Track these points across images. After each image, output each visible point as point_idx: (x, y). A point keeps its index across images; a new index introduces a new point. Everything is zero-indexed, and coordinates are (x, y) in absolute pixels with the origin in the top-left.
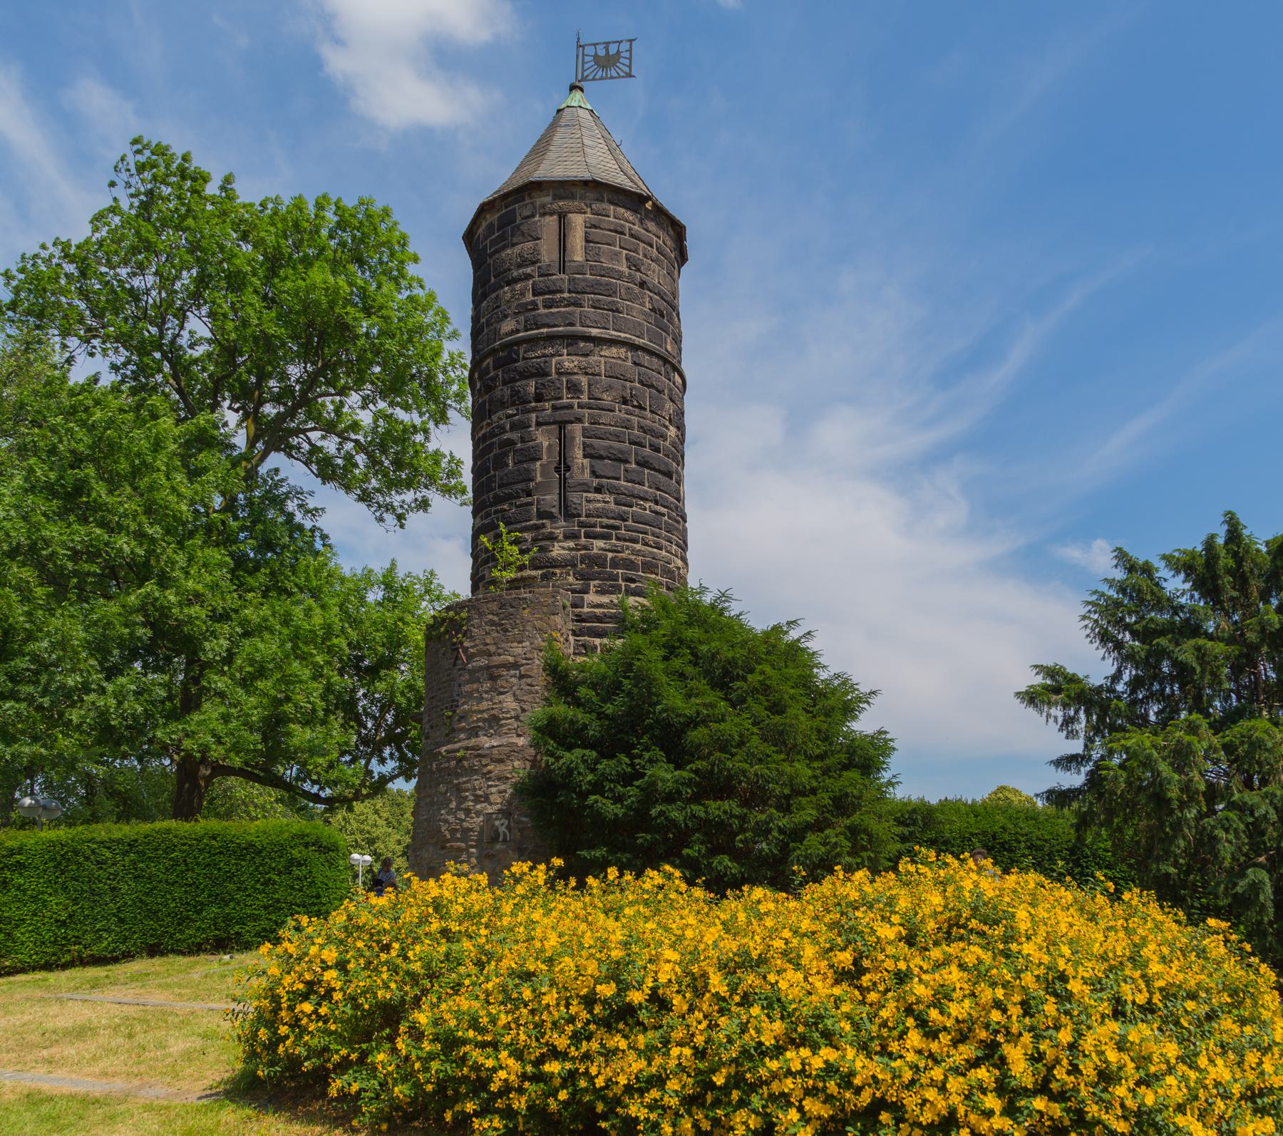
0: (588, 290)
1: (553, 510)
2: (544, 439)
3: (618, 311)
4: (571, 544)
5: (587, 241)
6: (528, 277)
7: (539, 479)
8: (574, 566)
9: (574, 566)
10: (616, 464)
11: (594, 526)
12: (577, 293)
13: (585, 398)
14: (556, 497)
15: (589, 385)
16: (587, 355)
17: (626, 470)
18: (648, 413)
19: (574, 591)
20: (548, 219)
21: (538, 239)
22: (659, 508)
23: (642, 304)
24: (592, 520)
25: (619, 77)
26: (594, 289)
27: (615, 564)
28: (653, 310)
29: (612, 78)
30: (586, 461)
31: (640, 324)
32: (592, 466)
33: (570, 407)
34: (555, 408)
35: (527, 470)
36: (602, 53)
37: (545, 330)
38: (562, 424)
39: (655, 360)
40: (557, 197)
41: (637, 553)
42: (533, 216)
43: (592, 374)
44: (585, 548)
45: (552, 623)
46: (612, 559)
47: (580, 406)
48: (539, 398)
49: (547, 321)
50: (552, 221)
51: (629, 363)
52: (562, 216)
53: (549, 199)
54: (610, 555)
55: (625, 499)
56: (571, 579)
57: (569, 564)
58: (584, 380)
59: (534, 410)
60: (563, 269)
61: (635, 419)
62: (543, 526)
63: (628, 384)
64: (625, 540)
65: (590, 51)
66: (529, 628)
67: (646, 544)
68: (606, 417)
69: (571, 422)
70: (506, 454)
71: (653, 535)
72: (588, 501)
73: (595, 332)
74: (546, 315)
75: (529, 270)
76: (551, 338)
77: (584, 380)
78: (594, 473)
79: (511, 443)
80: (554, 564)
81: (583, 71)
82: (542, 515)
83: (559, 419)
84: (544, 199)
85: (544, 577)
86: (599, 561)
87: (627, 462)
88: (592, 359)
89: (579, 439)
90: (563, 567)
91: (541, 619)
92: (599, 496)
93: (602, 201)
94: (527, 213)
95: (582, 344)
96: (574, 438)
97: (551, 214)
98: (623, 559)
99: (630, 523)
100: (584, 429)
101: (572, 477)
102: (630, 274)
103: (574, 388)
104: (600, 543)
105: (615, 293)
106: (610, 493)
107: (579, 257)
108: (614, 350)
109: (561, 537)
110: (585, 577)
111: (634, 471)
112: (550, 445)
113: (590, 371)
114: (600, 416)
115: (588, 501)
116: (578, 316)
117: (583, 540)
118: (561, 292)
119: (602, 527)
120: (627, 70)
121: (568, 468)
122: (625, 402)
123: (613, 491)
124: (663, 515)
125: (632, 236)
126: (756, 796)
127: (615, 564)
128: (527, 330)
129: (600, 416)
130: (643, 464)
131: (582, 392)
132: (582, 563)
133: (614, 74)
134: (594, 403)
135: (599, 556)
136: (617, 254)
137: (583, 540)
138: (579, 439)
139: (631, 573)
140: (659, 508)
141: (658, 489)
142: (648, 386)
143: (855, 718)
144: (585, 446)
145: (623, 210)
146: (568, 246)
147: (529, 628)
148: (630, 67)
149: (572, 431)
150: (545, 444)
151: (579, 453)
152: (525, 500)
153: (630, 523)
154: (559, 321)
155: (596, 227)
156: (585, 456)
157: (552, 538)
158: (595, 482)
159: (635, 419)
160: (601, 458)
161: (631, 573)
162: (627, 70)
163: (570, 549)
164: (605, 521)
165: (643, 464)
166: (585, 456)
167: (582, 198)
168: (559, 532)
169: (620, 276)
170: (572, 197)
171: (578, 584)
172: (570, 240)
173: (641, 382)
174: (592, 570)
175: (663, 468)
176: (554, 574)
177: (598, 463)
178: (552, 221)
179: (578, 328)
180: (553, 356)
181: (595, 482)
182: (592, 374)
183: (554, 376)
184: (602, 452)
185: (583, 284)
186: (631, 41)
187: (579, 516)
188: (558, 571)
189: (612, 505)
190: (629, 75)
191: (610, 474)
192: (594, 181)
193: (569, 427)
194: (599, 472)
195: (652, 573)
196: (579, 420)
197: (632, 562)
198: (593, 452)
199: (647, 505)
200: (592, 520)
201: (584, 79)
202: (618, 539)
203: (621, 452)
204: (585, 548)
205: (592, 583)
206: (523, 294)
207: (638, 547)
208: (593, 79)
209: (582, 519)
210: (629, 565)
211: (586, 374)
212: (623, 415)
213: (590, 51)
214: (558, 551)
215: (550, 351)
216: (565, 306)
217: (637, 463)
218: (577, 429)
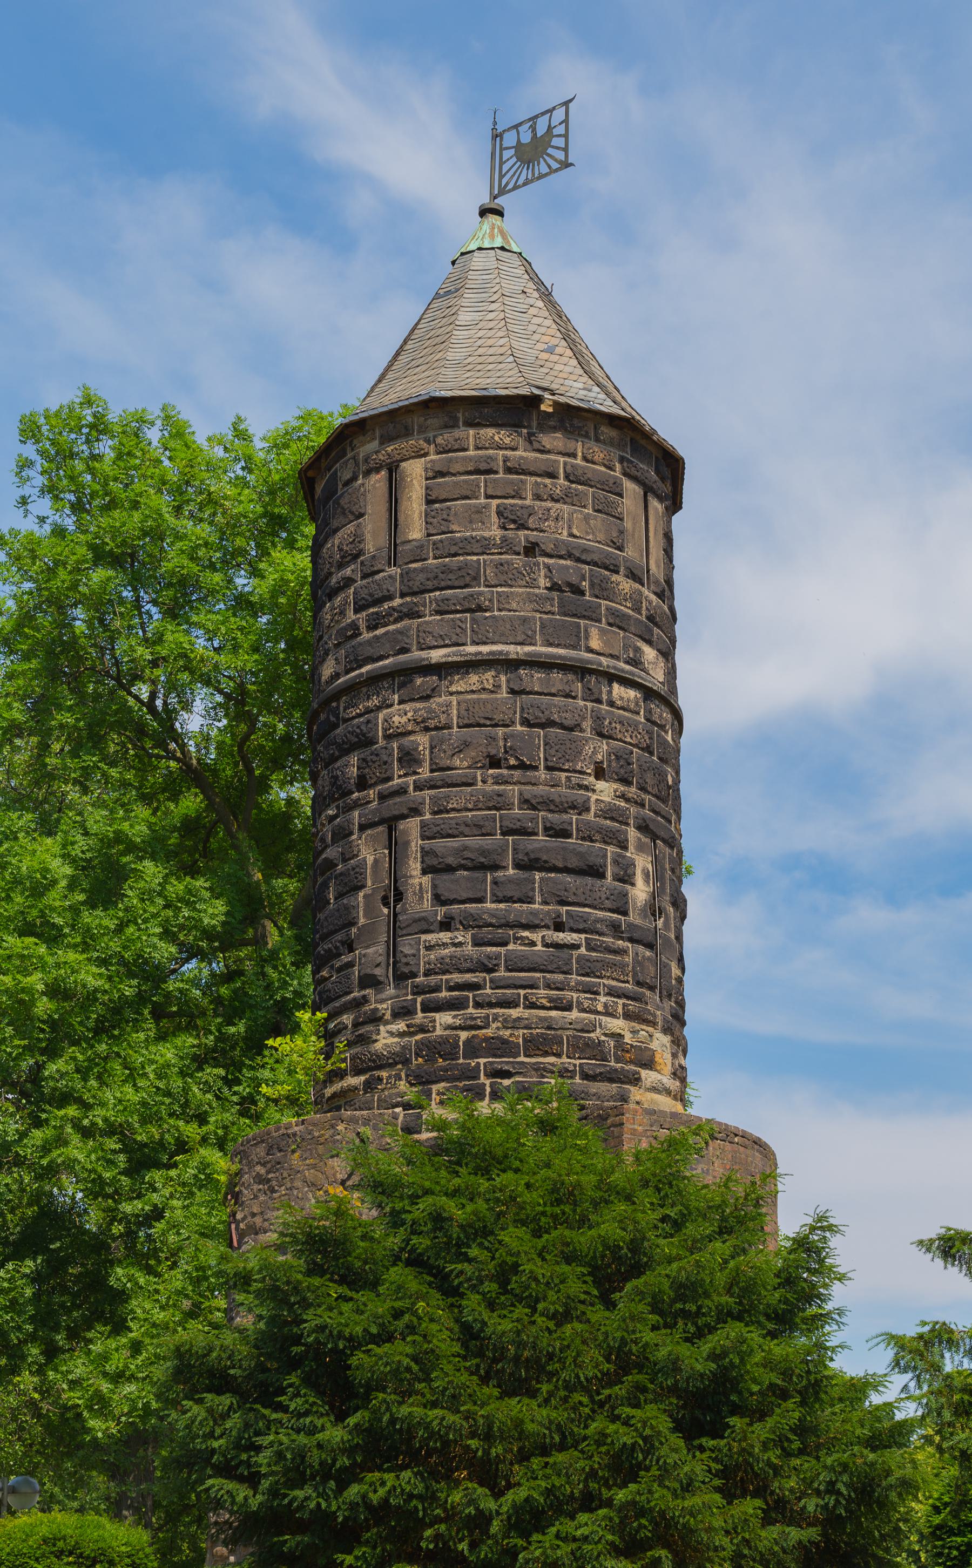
0: (430, 585)
1: (378, 971)
2: (369, 852)
3: (480, 609)
4: (401, 1026)
5: (429, 502)
6: (349, 581)
7: (362, 921)
8: (406, 1062)
9: (406, 1062)
10: (478, 874)
11: (437, 989)
12: (414, 594)
13: (425, 772)
14: (381, 949)
15: (432, 748)
16: (427, 698)
17: (495, 883)
18: (542, 774)
19: (407, 1106)
20: (375, 478)
21: (361, 515)
22: (561, 937)
23: (532, 584)
24: (433, 980)
25: (552, 171)
26: (439, 581)
27: (472, 1049)
28: (554, 587)
29: (541, 176)
30: (426, 880)
31: (525, 620)
32: (434, 886)
33: (402, 791)
34: (382, 797)
35: (347, 908)
36: (526, 138)
37: (368, 668)
38: (391, 823)
39: (556, 676)
40: (387, 439)
41: (515, 1024)
42: (354, 478)
43: (437, 728)
44: (422, 1029)
45: (329, 1172)
46: (468, 1042)
47: (418, 788)
48: (362, 784)
49: (369, 651)
50: (378, 480)
51: (504, 694)
52: (393, 469)
53: (375, 445)
54: (464, 1035)
55: (490, 932)
56: (403, 1085)
57: (399, 1059)
58: (422, 741)
59: (356, 805)
60: (393, 560)
61: (513, 791)
62: (365, 1000)
63: (500, 731)
64: (491, 1005)
65: (510, 139)
66: (298, 1184)
67: (533, 1006)
68: (458, 797)
69: (404, 817)
70: (325, 885)
71: (548, 986)
72: (429, 948)
73: (436, 655)
74: (369, 642)
75: (348, 572)
76: (374, 680)
77: (422, 741)
78: (439, 900)
79: (331, 864)
80: (379, 1063)
81: (501, 176)
82: (369, 981)
83: (386, 814)
84: (368, 448)
85: (369, 1086)
86: (443, 1049)
87: (496, 867)
88: (435, 703)
89: (416, 843)
90: (391, 1066)
91: (314, 1166)
92: (445, 936)
93: (455, 426)
94: (347, 476)
95: (419, 681)
96: (407, 843)
97: (377, 470)
98: (487, 1039)
99: (502, 973)
100: (424, 825)
101: (404, 910)
102: (504, 539)
103: (409, 759)
104: (445, 1018)
105: (476, 578)
106: (466, 928)
107: (415, 532)
108: (474, 678)
109: (388, 1016)
110: (423, 1080)
111: (510, 880)
112: (376, 861)
113: (431, 723)
114: (447, 798)
115: (429, 948)
116: (414, 632)
117: (420, 1017)
118: (390, 598)
119: (450, 989)
120: (560, 155)
121: (399, 896)
122: (495, 762)
123: (469, 923)
124: (576, 947)
125: (509, 470)
126: (438, 1458)
127: (472, 1049)
128: (347, 672)
129: (447, 798)
130: (528, 864)
131: (419, 763)
132: (417, 1055)
133: (544, 169)
134: (444, 779)
135: (444, 1040)
136: (479, 511)
137: (420, 1017)
138: (416, 843)
139: (502, 1062)
140: (561, 937)
141: (563, 903)
142: (542, 726)
143: (796, 1291)
144: (425, 853)
145: (490, 431)
146: (401, 518)
147: (298, 1184)
148: (566, 150)
149: (406, 832)
150: (370, 860)
151: (415, 867)
152: (345, 959)
153: (502, 973)
154: (386, 648)
155: (442, 474)
156: (424, 872)
157: (376, 1019)
158: (441, 911)
159: (513, 791)
160: (450, 869)
161: (502, 1062)
162: (560, 155)
163: (401, 1035)
164: (457, 978)
165: (528, 864)
166: (424, 872)
167: (422, 430)
168: (385, 1008)
169: (485, 546)
170: (407, 433)
171: (410, 1093)
172: (403, 505)
173: (526, 722)
174: (435, 1063)
175: (573, 863)
176: (380, 1079)
177: (445, 879)
178: (378, 480)
179: (416, 654)
180: (379, 708)
181: (441, 911)
182: (437, 728)
183: (381, 742)
184: (450, 860)
185: (421, 577)
186: (566, 104)
187: (414, 975)
188: (384, 1074)
189: (469, 949)
190: (566, 165)
191: (465, 895)
192: (433, 400)
193: (402, 825)
194: (446, 895)
195: (546, 1054)
196: (415, 811)
197: (505, 1042)
198: (434, 862)
199: (536, 936)
200: (433, 980)
201: (503, 191)
202: (478, 1005)
203: (483, 852)
204: (422, 1029)
205: (435, 1088)
206: (342, 613)
207: (515, 1013)
208: (516, 187)
209: (420, 979)
210: (500, 1047)
211: (427, 729)
212: (490, 788)
213: (510, 139)
214: (386, 1039)
215: (375, 701)
216: (396, 621)
217: (517, 866)
218: (412, 826)
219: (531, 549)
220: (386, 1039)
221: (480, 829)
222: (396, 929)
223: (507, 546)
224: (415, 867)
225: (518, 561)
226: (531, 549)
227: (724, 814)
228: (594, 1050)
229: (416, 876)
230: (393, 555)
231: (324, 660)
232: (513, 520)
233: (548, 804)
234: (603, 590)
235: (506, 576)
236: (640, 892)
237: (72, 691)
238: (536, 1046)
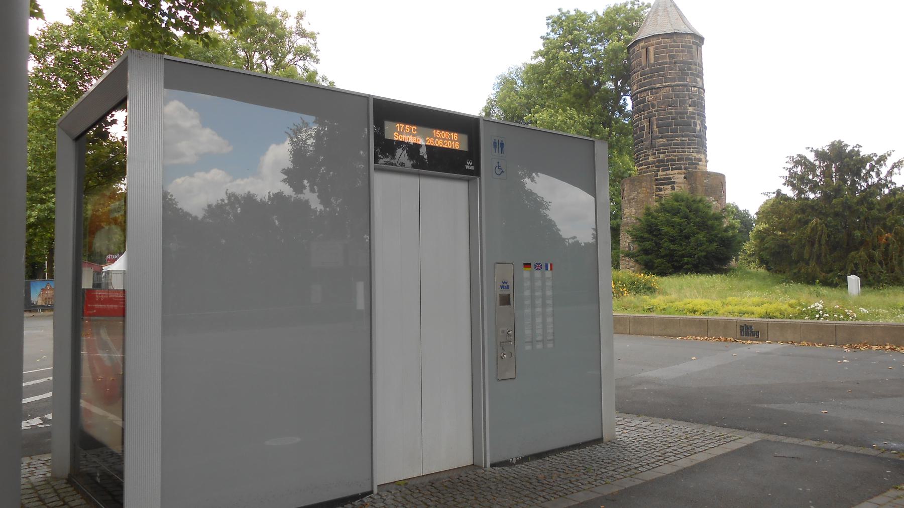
57: (654, 163)
73: (657, 86)
86: (662, 161)
103: (653, 106)
151: (655, 127)
157: (648, 155)
169: (666, 63)
214: (651, 159)
219: (675, 63)
220: (651, 159)
221: (668, 119)
222: (652, 138)
223: (670, 63)
224: (655, 127)
225: (672, 65)
226: (675, 63)
227: (24, 390)
228: (691, 159)
229: (655, 128)
230: (648, 64)
231: (755, 431)
232: (671, 57)
233: (680, 113)
234: (689, 69)
235: (670, 69)
236: (698, 128)
237: (857, 249)
238: (679, 160)
